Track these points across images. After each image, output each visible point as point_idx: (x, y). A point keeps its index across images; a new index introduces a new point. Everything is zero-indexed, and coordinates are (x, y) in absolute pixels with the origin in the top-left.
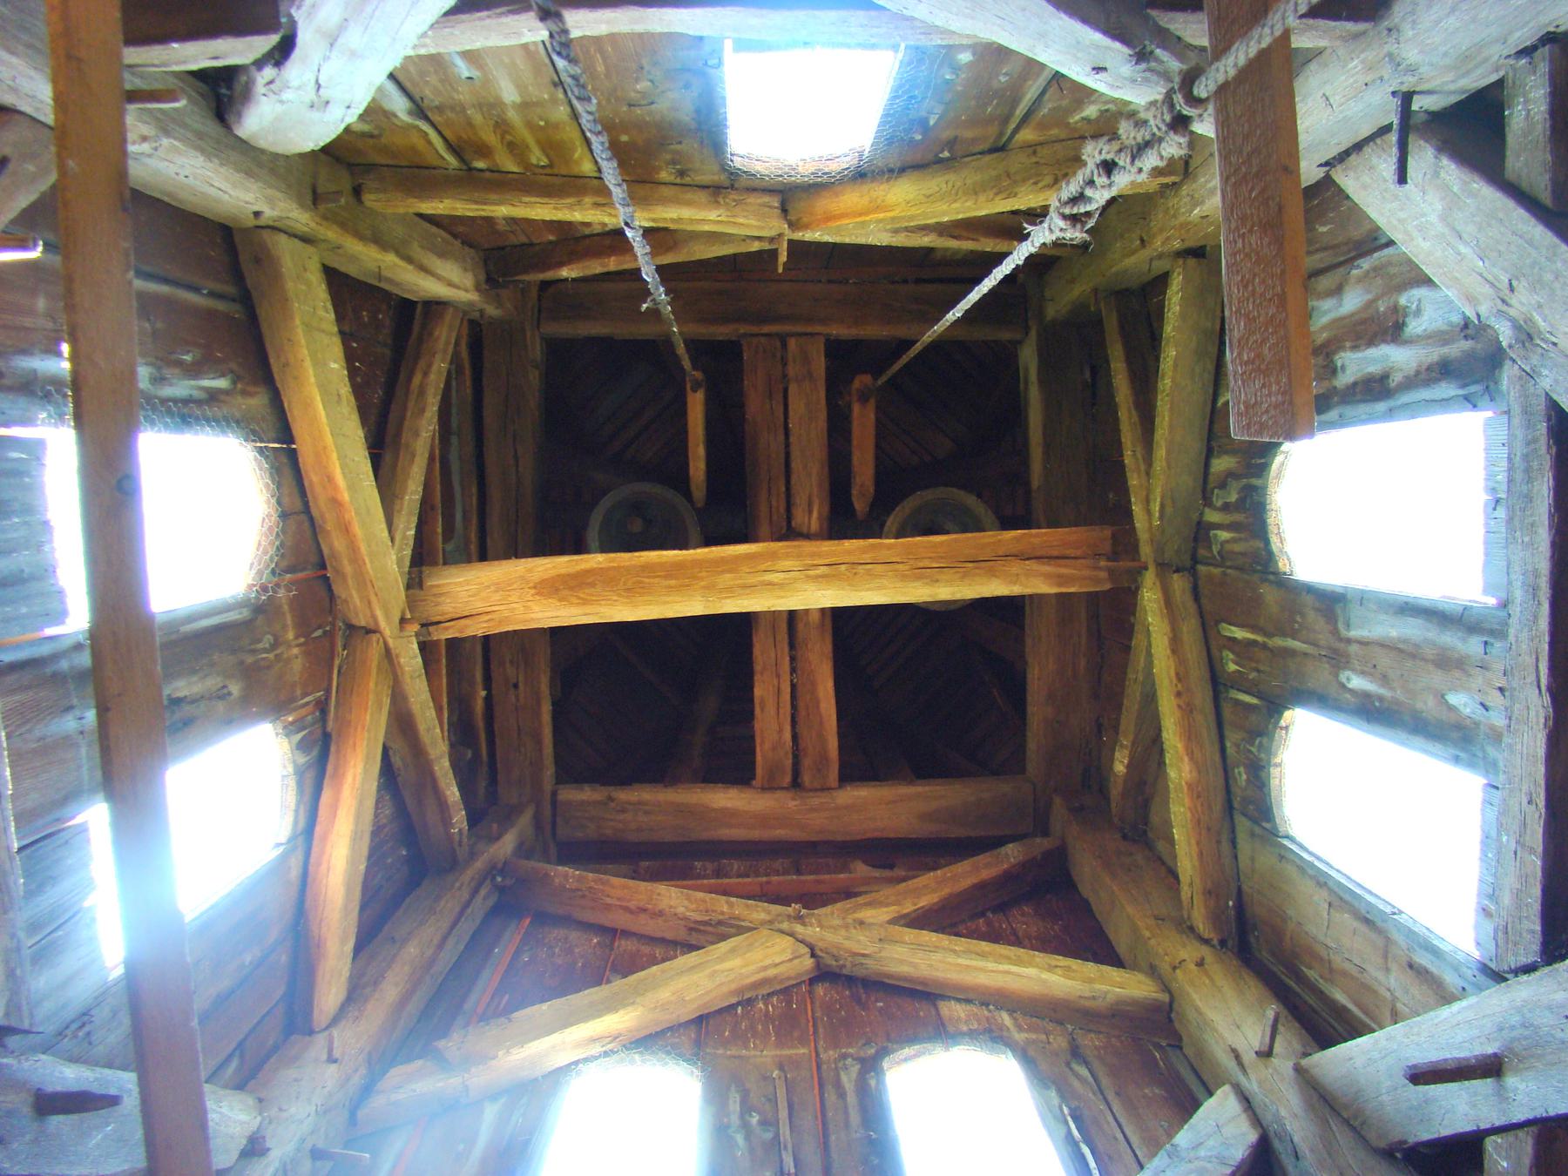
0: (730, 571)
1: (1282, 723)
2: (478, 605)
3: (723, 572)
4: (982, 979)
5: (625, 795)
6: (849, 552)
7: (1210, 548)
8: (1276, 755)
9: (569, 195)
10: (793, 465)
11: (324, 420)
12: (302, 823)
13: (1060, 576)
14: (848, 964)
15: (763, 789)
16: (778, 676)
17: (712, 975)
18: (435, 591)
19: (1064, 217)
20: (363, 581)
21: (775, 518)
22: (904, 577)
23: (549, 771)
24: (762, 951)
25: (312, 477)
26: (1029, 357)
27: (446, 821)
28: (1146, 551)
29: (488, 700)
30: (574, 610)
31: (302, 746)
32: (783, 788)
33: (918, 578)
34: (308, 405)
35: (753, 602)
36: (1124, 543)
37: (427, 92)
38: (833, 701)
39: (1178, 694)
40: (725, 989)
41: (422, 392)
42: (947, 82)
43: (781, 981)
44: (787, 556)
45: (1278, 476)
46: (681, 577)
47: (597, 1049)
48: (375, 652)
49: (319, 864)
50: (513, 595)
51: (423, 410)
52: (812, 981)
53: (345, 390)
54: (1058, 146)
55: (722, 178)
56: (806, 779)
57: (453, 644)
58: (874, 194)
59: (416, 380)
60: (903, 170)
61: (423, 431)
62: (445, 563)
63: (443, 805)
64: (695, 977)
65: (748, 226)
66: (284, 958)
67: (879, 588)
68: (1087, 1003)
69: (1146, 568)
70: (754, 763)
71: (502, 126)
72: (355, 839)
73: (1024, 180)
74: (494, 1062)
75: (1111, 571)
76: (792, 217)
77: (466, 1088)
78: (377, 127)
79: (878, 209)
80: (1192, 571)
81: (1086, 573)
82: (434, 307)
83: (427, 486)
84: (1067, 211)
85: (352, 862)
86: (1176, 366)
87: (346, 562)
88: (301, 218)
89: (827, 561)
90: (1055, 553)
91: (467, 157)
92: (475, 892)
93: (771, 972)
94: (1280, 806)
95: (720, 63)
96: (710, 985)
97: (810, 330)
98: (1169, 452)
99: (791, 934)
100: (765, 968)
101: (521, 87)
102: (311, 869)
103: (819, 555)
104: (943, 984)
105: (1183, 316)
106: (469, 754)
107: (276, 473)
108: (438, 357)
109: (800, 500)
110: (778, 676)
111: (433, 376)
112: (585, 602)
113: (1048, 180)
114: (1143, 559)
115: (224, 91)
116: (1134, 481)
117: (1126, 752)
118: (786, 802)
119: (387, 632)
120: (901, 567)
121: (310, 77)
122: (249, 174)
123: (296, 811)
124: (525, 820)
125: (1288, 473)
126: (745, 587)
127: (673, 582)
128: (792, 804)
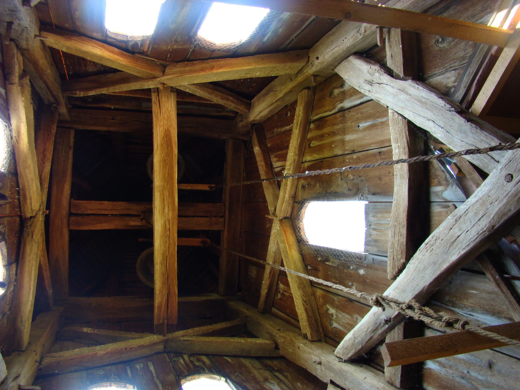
0: (169, 195)
1: (128, 385)
2: (163, 110)
3: (169, 193)
4: (26, 279)
5: (71, 153)
7: (174, 357)
8: (114, 384)
9: (299, 152)
11: (243, 68)
12: (109, 40)
13: (161, 307)
14: (28, 230)
15: (70, 203)
16: (111, 210)
17: (32, 180)
18: (169, 96)
19: (377, 299)
20: (182, 73)
22: (164, 254)
23: (81, 127)
24: (35, 199)
25: (222, 62)
26: (214, 297)
27: (81, 90)
28: (170, 336)
29: (110, 109)
30: (159, 142)
31: (136, 44)
32: (70, 209)
33: (163, 259)
34: (249, 64)
35: (158, 202)
36: (172, 329)
37: (352, 113)
38: (101, 229)
39: (126, 349)
40: (26, 184)
41: (228, 100)
42: (349, 267)
43: (24, 205)
44: (173, 214)
45: (211, 378)
46: (168, 179)
47: (14, 135)
48: (157, 73)
49: (95, 43)
50: (165, 121)
51: (222, 99)
52: (21, 217)
53: (248, 76)
54: (315, 302)
55: (300, 199)
56: (73, 218)
57: (150, 100)
58: (294, 246)
59: (231, 98)
60: (301, 254)
61: (216, 99)
62: (177, 101)
63: (90, 89)
64: (33, 173)
65: (282, 206)
66: (67, 25)
67: (161, 245)
68: (19, 319)
69: (164, 336)
70: (80, 200)
71: (333, 134)
72: (101, 58)
73: (304, 292)
74: (20, 95)
75: (163, 324)
76: (284, 220)
77: (12, 84)
78: (335, 97)
79: (289, 247)
80: (164, 352)
81: (162, 316)
82: (249, 106)
83: (200, 98)
84: (379, 299)
85: (95, 55)
86: (238, 342)
87: (190, 68)
88: (311, 70)
89: (171, 227)
90: (169, 305)
91: (316, 122)
92: (53, 96)
93: (28, 201)
94: (96, 387)
95: (360, 199)
96: (29, 179)
97: (226, 225)
98: (208, 341)
99: (39, 210)
100: (31, 199)
101: (353, 141)
102: (94, 41)
104: (23, 265)
105: (256, 344)
106: (90, 100)
107: (228, 50)
108: (235, 106)
110: (111, 210)
111: (230, 104)
112: (162, 146)
113: (305, 299)
114: (167, 335)
115: (365, 55)
116: (190, 331)
117: (92, 332)
118: (65, 211)
119: (162, 78)
120: (167, 252)
121: (385, 81)
122: (335, 58)
123: (115, 39)
124: (67, 117)
125: (215, 381)
126: (164, 200)
127: (167, 175)
128: (64, 212)
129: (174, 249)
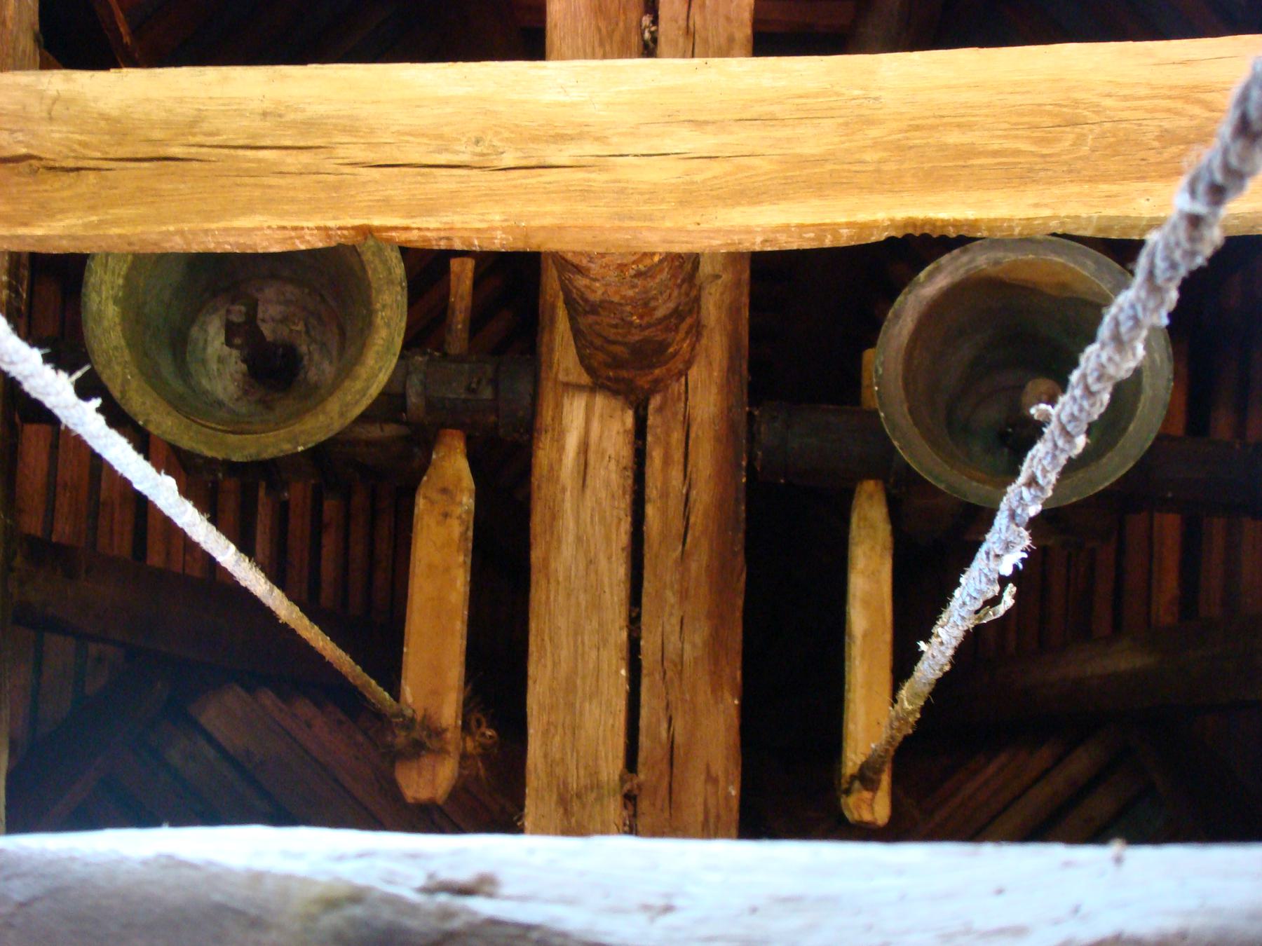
0: (803, 161)
3: (820, 160)
6: (492, 196)
10: (620, 570)
21: (677, 436)
33: (310, 125)
44: (652, 194)
103: (567, 192)
109: (610, 475)
126: (801, 97)
127: (954, 138)
129: (386, 204)
